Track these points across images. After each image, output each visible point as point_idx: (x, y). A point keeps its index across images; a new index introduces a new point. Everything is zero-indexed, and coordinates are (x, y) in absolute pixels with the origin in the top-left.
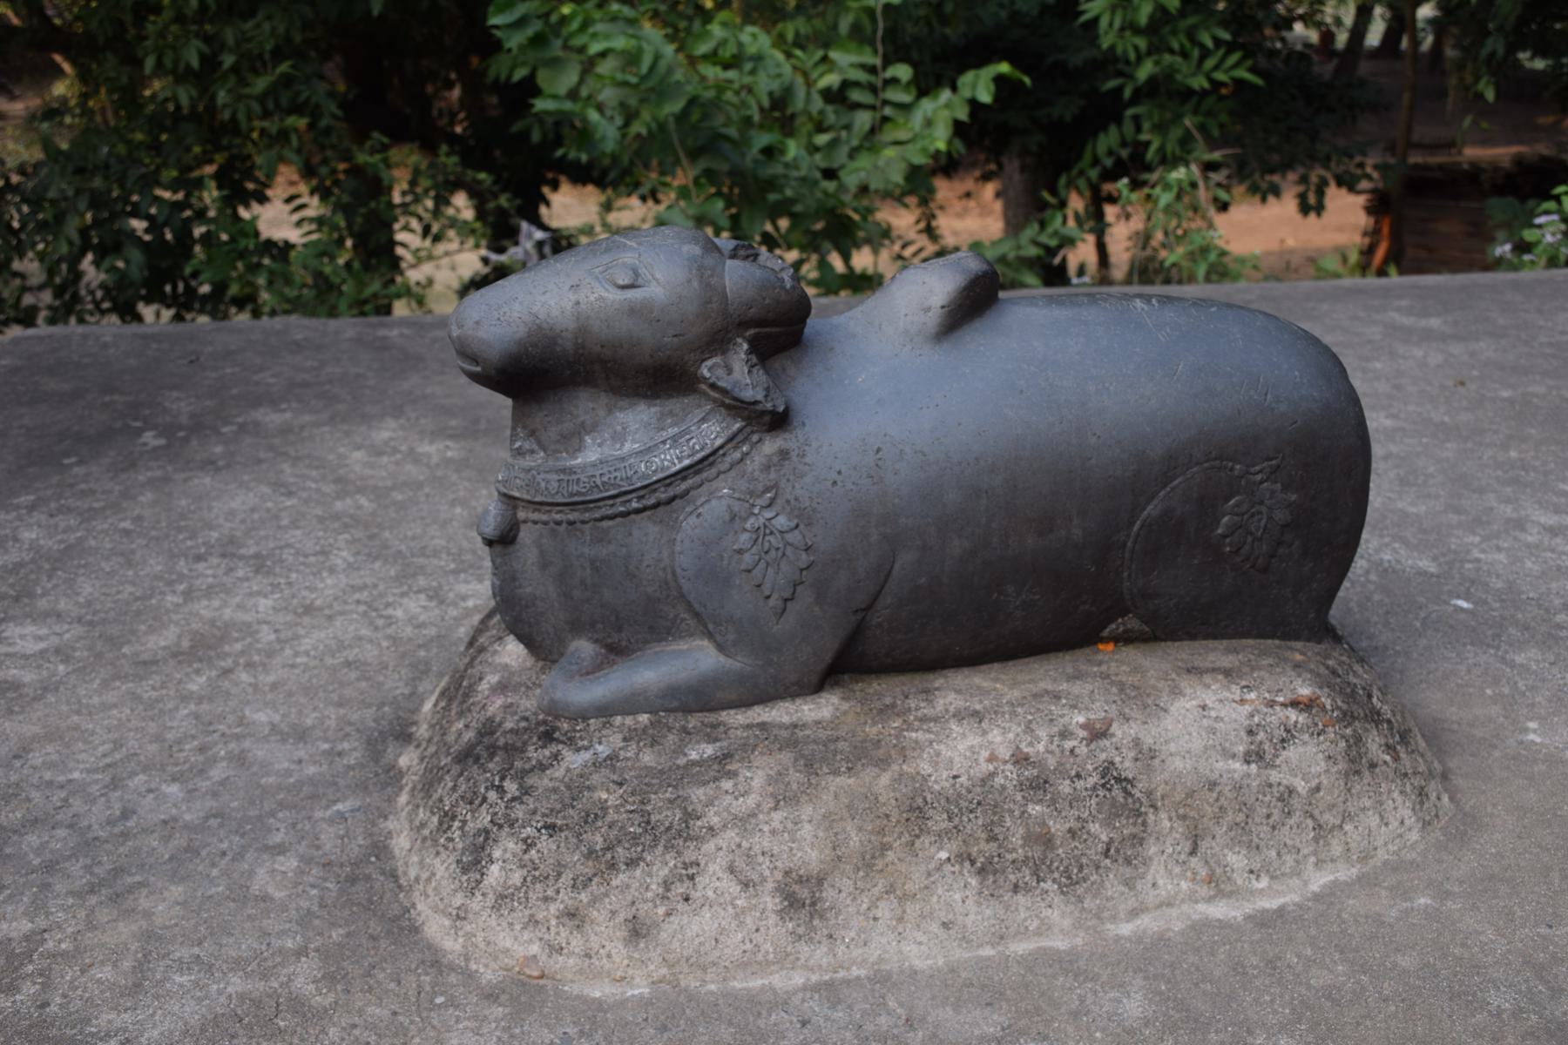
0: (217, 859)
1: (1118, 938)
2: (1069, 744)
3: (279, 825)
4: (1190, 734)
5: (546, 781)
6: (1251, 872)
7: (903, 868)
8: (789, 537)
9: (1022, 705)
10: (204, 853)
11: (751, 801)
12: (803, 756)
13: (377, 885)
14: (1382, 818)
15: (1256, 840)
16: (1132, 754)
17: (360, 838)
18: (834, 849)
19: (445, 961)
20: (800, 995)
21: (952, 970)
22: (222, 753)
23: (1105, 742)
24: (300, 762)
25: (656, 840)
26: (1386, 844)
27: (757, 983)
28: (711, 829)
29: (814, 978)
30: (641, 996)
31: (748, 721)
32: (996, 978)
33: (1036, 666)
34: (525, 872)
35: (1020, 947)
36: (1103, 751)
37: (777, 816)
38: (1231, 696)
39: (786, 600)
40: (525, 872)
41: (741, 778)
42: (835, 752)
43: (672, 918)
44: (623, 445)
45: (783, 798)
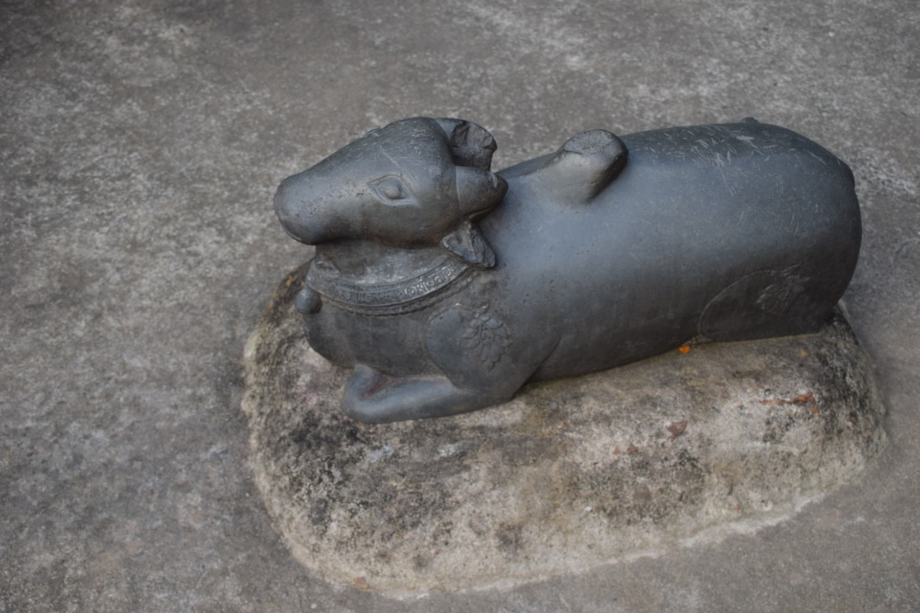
0: (149, 497)
1: (686, 549)
2: (661, 441)
3: (180, 466)
4: (732, 428)
6: (763, 501)
7: (566, 517)
8: (498, 332)
9: (634, 411)
10: (139, 491)
11: (479, 485)
12: (507, 453)
13: (256, 517)
14: (842, 461)
15: (767, 483)
16: (697, 444)
17: (235, 476)
18: (527, 510)
19: (310, 576)
20: (512, 596)
21: (595, 576)
22: (122, 399)
23: (682, 438)
24: (176, 407)
25: (427, 510)
26: (843, 475)
27: (488, 587)
28: (458, 502)
29: (519, 583)
30: (425, 599)
31: (472, 424)
32: (619, 581)
33: (641, 369)
34: (352, 529)
35: (631, 558)
36: (680, 443)
37: (495, 493)
38: (758, 398)
39: (494, 363)
40: (352, 529)
41: (473, 471)
42: (526, 449)
43: (439, 555)
44: (392, 276)
45: (498, 482)
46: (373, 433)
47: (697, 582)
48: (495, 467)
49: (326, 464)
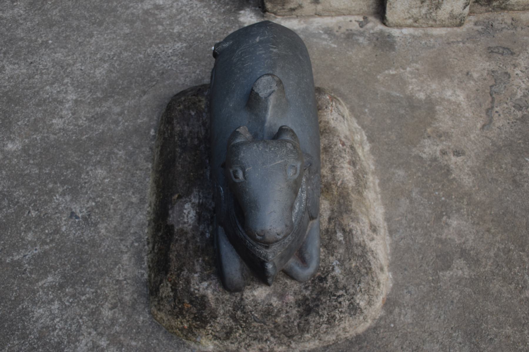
5: (343, 281)
12: (346, 211)
19: (374, 326)
21: (386, 205)
25: (364, 256)
29: (387, 234)
46: (324, 268)
47: (392, 170)
48: (352, 218)
49: (333, 298)
